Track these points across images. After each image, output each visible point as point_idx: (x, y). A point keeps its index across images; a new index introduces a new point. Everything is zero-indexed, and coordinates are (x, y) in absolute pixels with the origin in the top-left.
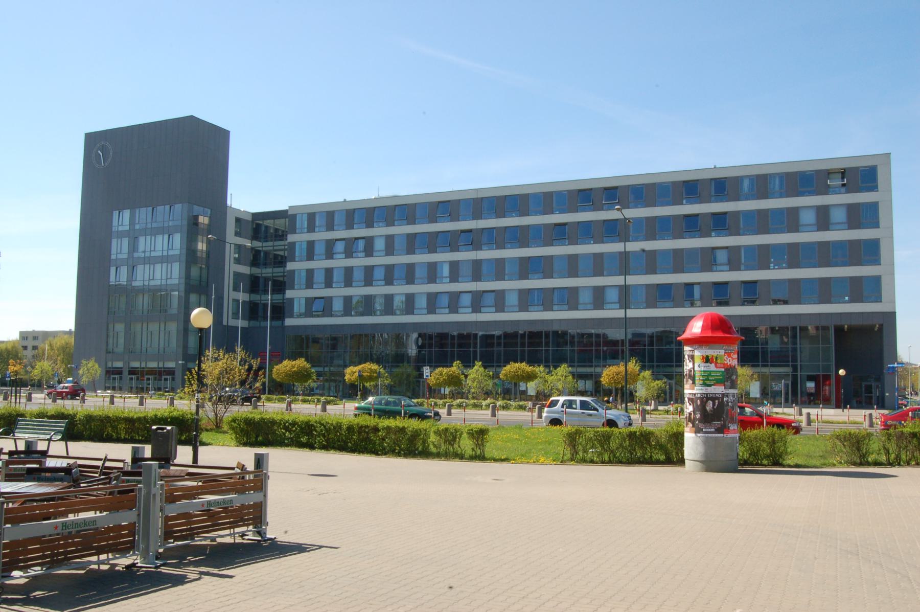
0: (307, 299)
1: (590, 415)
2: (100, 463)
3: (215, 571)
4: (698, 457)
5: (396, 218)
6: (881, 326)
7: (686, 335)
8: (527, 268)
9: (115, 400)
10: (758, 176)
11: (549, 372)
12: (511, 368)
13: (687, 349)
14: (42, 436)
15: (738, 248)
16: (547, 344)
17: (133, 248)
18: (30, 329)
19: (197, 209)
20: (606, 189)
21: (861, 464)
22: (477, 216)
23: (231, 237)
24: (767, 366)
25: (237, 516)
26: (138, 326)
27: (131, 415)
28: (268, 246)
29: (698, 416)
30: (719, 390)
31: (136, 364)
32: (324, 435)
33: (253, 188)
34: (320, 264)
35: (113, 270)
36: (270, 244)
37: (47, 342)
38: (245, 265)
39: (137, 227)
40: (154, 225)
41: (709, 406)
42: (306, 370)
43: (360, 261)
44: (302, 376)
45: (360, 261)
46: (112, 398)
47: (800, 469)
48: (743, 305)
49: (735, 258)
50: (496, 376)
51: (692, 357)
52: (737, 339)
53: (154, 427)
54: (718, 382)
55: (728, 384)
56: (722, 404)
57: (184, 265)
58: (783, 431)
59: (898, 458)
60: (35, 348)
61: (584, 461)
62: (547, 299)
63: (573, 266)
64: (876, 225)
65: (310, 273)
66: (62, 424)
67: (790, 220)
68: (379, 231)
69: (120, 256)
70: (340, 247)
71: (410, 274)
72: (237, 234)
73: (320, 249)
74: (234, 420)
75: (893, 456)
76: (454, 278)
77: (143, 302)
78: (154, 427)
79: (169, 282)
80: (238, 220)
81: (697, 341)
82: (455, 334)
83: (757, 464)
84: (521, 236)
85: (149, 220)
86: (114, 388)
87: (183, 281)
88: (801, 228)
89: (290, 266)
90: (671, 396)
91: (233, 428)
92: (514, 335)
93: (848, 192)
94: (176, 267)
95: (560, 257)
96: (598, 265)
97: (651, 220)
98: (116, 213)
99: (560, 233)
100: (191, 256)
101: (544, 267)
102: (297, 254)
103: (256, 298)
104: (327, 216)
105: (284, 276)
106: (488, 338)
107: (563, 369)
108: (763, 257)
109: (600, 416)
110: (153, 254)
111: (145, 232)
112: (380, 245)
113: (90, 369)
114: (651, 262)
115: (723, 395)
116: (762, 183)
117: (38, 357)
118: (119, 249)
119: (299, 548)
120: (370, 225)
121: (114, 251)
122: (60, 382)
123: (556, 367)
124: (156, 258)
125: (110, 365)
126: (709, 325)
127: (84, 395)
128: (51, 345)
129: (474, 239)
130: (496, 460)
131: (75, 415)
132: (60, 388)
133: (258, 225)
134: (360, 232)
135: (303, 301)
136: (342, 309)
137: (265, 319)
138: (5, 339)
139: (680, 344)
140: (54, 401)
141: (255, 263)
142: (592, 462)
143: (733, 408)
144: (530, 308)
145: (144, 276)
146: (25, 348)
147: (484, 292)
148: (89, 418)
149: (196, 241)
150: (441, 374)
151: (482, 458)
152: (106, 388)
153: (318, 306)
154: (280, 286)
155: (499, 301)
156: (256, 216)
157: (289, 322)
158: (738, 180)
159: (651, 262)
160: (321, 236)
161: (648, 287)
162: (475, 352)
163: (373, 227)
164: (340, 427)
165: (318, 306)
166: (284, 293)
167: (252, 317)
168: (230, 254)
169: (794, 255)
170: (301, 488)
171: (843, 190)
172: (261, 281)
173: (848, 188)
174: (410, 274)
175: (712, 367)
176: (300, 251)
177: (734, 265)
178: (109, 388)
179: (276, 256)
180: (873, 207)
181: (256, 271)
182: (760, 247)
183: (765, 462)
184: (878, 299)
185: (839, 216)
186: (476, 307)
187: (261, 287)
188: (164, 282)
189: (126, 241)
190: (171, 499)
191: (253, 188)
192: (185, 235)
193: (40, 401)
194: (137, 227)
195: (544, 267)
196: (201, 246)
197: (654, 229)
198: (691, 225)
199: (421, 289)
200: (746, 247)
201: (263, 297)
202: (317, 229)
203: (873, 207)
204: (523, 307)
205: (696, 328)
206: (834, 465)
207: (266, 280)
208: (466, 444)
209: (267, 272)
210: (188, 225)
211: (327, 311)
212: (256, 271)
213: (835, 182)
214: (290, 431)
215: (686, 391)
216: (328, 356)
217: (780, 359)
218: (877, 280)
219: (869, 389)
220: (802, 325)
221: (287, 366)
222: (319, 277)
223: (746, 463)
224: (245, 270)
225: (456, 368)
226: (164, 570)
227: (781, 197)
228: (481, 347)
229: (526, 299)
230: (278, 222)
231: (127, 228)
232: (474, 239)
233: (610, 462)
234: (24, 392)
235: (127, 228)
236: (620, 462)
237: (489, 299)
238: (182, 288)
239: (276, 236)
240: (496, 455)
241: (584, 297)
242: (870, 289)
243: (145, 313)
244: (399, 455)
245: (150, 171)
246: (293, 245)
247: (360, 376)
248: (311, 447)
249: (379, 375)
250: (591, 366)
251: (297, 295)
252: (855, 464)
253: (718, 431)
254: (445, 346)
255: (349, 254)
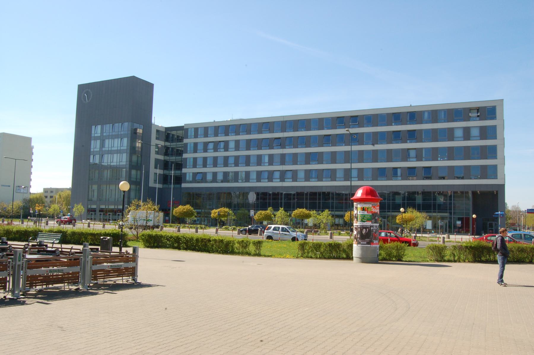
0: (193, 173)
1: (286, 234)
2: (69, 250)
3: (111, 292)
4: (358, 256)
5: (241, 131)
6: (497, 192)
7: (354, 197)
8: (309, 158)
9: (91, 225)
10: (432, 111)
11: (319, 214)
12: (298, 211)
13: (355, 204)
14: (50, 241)
15: (421, 149)
16: (319, 199)
17: (102, 145)
18: (49, 187)
19: (136, 125)
20: (352, 117)
21: (441, 261)
22: (283, 130)
23: (154, 141)
24: (436, 212)
25: (119, 272)
26: (105, 186)
27: (94, 232)
28: (173, 145)
29: (359, 236)
30: (369, 224)
31: (103, 207)
32: (185, 243)
33: (163, 117)
34: (200, 155)
35: (92, 157)
36: (174, 144)
37: (58, 194)
38: (161, 155)
39: (105, 134)
40: (114, 133)
41: (364, 231)
42: (191, 211)
43: (221, 154)
44: (189, 214)
45: (221, 154)
46: (89, 224)
47: (410, 263)
48: (424, 179)
49: (419, 155)
50: (290, 216)
51: (357, 208)
52: (378, 200)
53: (102, 237)
54: (368, 220)
55: (373, 221)
56: (370, 231)
57: (129, 154)
58: (403, 245)
59: (459, 258)
60: (51, 197)
61: (308, 257)
62: (320, 175)
63: (333, 158)
64: (495, 138)
65: (195, 159)
66: (59, 236)
67: (450, 135)
68: (232, 138)
69: (95, 150)
70: (211, 146)
71: (248, 161)
72: (157, 138)
73: (200, 147)
74: (143, 235)
75: (456, 258)
76: (271, 163)
77: (107, 174)
78: (102, 237)
79: (121, 163)
80: (158, 131)
81: (360, 200)
82: (271, 193)
83: (390, 260)
84: (306, 142)
85: (111, 131)
86: (91, 219)
87: (128, 163)
88: (455, 139)
89: (185, 156)
90: (348, 226)
91: (143, 239)
92: (315, 194)
93: (480, 120)
94: (125, 155)
95: (327, 153)
96: (348, 157)
97: (375, 134)
98: (93, 127)
99: (327, 140)
100: (132, 150)
101: (318, 158)
102: (188, 150)
103: (167, 172)
104: (205, 130)
105: (181, 161)
106: (288, 196)
107: (326, 212)
108: (434, 154)
109: (290, 235)
110: (113, 149)
111: (108, 137)
112: (232, 145)
113: (79, 209)
114: (375, 156)
115: (371, 226)
116: (435, 115)
117: (52, 202)
118: (95, 146)
119: (149, 286)
120: (227, 134)
121: (92, 147)
122: (64, 215)
123: (322, 211)
124: (114, 151)
125: (89, 207)
126: (413, 191)
127: (76, 222)
128: (60, 196)
129: (282, 143)
130: (265, 256)
131: (67, 232)
132: (63, 218)
133: (168, 134)
134: (221, 138)
135: (191, 174)
136: (211, 179)
137: (171, 184)
138: (36, 192)
139: (353, 201)
140: (60, 225)
141: (166, 154)
142: (311, 258)
143: (375, 232)
144: (311, 180)
145: (107, 160)
146: (46, 197)
147: (286, 171)
148: (74, 233)
149: (135, 142)
150: (261, 214)
151: (259, 255)
152: (87, 219)
153: (199, 177)
154: (179, 166)
155: (295, 175)
156: (167, 129)
157: (184, 185)
158: (421, 113)
159: (375, 156)
160: (201, 140)
161: (373, 169)
162: (281, 203)
163: (228, 135)
164: (193, 239)
165: (199, 177)
166: (181, 170)
167: (165, 181)
168: (153, 149)
169: (451, 154)
170: (151, 262)
171: (478, 118)
172: (170, 163)
173: (481, 118)
174: (248, 161)
175: (366, 213)
176: (190, 148)
177: (419, 158)
178: (89, 219)
179: (178, 150)
180: (494, 128)
181: (167, 158)
182: (433, 149)
183: (394, 259)
184: (496, 177)
185: (475, 132)
186: (282, 179)
187: (170, 167)
188: (118, 164)
189: (98, 142)
190: (95, 263)
191: (163, 117)
192: (130, 139)
193: (53, 224)
194: (105, 134)
195: (318, 158)
196: (138, 144)
197: (376, 138)
198: (397, 136)
199: (253, 169)
200: (426, 149)
201: (170, 172)
202: (199, 136)
203: (494, 128)
204: (307, 179)
205: (359, 194)
206: (428, 261)
207: (172, 162)
208: (252, 248)
209: (173, 159)
210: (131, 134)
211: (204, 179)
212: (167, 158)
213: (474, 114)
214: (169, 241)
215: (354, 224)
216: (202, 204)
217: (441, 208)
218: (495, 167)
219: (491, 225)
220: (455, 190)
221: (180, 209)
222: (200, 162)
223: (384, 259)
224: (161, 157)
225: (269, 211)
226: (90, 291)
227: (445, 122)
228: (284, 200)
229: (308, 175)
230: (179, 132)
231: (99, 135)
232: (282, 143)
233: (320, 258)
234: (44, 220)
235: (99, 135)
236: (325, 258)
237: (289, 175)
238: (128, 166)
239: (178, 140)
240: (267, 254)
241: (340, 174)
242: (491, 172)
243: (108, 179)
244: (220, 253)
245: (112, 106)
246: (186, 145)
247: (219, 215)
248: (179, 249)
249: (229, 214)
250: (342, 211)
251: (188, 171)
252: (438, 261)
253: (368, 243)
254: (269, 200)
255: (216, 149)
